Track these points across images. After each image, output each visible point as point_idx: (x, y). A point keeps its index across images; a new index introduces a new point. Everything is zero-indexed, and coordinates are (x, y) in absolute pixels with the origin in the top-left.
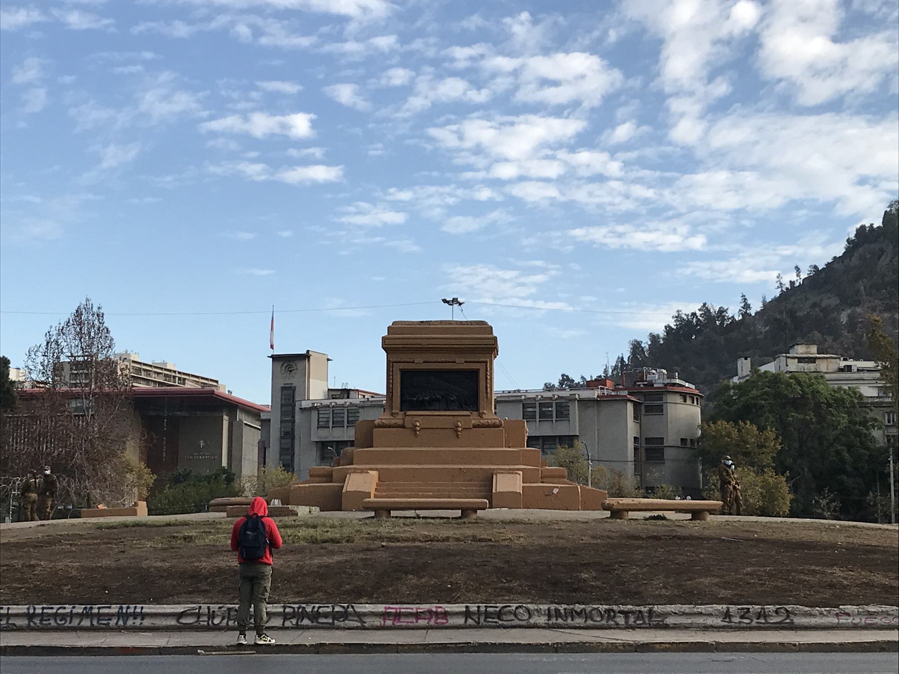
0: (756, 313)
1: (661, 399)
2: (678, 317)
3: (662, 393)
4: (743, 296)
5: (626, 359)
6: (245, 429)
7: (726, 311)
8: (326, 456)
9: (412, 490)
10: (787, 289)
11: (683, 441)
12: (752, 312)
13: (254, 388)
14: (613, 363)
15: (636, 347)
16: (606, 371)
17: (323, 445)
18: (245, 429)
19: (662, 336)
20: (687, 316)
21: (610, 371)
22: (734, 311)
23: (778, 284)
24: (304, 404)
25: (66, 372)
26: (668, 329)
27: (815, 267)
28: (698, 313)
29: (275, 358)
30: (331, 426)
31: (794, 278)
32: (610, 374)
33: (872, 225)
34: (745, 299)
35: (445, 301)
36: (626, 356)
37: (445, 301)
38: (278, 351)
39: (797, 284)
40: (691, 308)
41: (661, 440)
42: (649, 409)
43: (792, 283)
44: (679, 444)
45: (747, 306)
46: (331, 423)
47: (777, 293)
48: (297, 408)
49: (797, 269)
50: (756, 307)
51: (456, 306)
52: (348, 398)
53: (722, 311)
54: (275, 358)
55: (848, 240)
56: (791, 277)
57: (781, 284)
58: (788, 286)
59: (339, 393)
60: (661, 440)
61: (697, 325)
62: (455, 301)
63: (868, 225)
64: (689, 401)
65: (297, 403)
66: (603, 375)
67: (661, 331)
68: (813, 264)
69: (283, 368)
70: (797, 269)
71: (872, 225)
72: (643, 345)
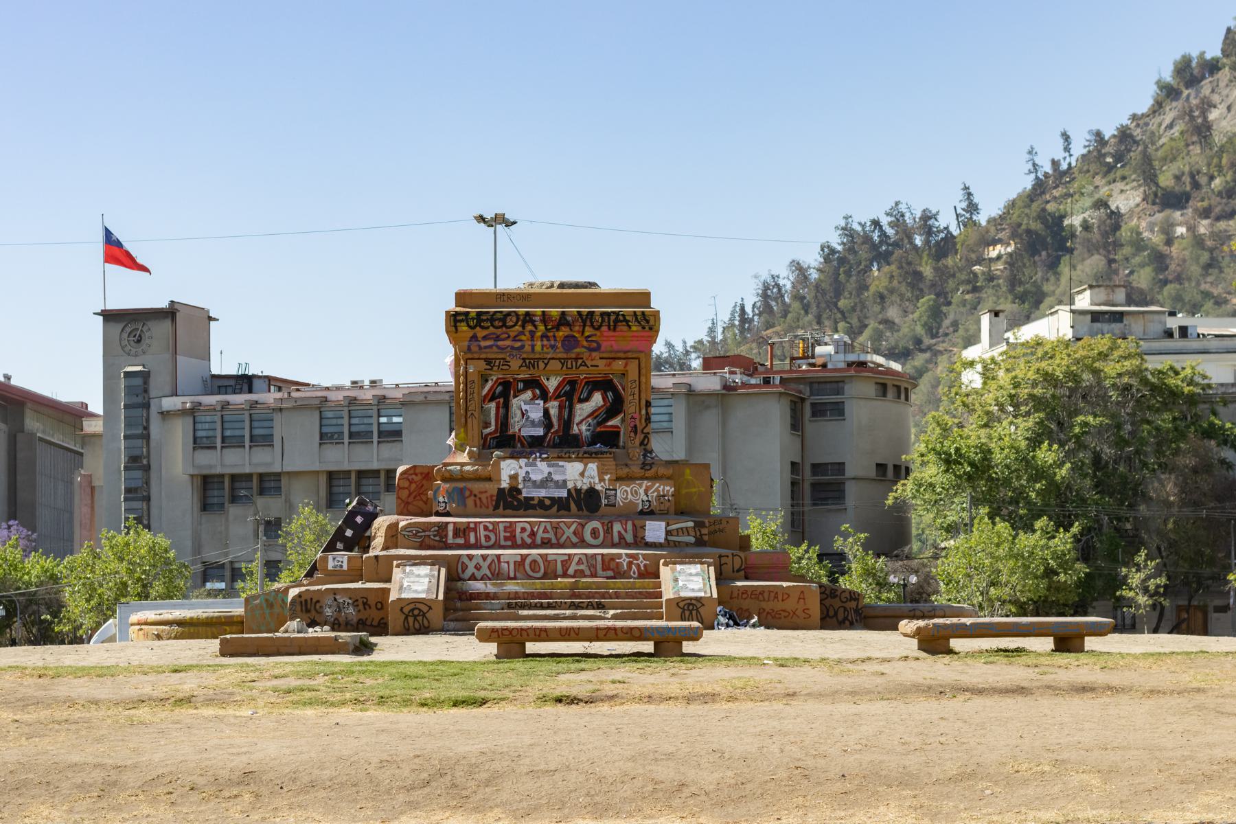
0: (989, 222)
1: (839, 392)
2: (847, 231)
3: (841, 381)
4: (966, 188)
5: (749, 309)
6: (40, 447)
7: (935, 217)
8: (210, 501)
9: (545, 596)
10: (1046, 175)
11: (881, 467)
12: (982, 218)
13: (72, 372)
14: (724, 316)
15: (770, 292)
16: (712, 331)
17: (206, 483)
18: (40, 447)
19: (814, 264)
20: (863, 225)
21: (720, 330)
22: (947, 220)
23: (1030, 166)
24: (170, 403)
25: (853, 604)
26: (828, 253)
27: (1098, 134)
28: (885, 221)
29: (109, 316)
30: (219, 445)
31: (1059, 154)
32: (720, 337)
33: (1203, 53)
34: (970, 194)
35: (481, 219)
36: (751, 300)
37: (481, 219)
38: (113, 305)
39: (1064, 166)
40: (869, 208)
41: (840, 467)
42: (819, 411)
43: (1055, 164)
44: (872, 473)
45: (972, 207)
46: (219, 440)
47: (1028, 183)
48: (154, 410)
49: (1066, 137)
50: (989, 209)
51: (500, 228)
52: (250, 391)
53: (927, 217)
54: (109, 316)
55: (1158, 83)
56: (1050, 152)
57: (1034, 165)
58: (1048, 168)
59: (232, 382)
60: (840, 467)
61: (881, 242)
62: (501, 220)
63: (1195, 54)
64: (891, 393)
65: (153, 402)
66: (706, 339)
67: (812, 259)
68: (1095, 128)
69: (125, 335)
70: (1066, 137)
71: (1203, 53)
72: (781, 282)
